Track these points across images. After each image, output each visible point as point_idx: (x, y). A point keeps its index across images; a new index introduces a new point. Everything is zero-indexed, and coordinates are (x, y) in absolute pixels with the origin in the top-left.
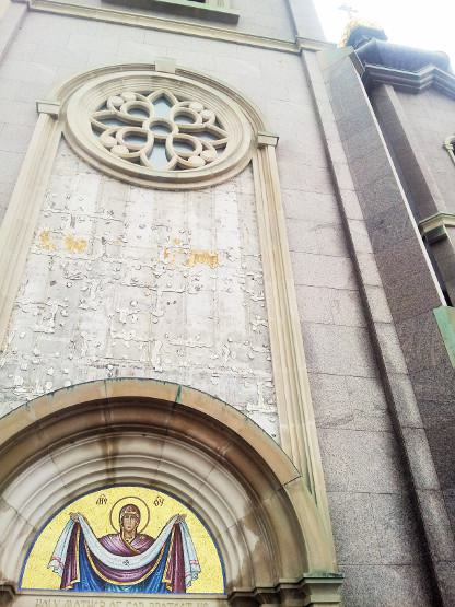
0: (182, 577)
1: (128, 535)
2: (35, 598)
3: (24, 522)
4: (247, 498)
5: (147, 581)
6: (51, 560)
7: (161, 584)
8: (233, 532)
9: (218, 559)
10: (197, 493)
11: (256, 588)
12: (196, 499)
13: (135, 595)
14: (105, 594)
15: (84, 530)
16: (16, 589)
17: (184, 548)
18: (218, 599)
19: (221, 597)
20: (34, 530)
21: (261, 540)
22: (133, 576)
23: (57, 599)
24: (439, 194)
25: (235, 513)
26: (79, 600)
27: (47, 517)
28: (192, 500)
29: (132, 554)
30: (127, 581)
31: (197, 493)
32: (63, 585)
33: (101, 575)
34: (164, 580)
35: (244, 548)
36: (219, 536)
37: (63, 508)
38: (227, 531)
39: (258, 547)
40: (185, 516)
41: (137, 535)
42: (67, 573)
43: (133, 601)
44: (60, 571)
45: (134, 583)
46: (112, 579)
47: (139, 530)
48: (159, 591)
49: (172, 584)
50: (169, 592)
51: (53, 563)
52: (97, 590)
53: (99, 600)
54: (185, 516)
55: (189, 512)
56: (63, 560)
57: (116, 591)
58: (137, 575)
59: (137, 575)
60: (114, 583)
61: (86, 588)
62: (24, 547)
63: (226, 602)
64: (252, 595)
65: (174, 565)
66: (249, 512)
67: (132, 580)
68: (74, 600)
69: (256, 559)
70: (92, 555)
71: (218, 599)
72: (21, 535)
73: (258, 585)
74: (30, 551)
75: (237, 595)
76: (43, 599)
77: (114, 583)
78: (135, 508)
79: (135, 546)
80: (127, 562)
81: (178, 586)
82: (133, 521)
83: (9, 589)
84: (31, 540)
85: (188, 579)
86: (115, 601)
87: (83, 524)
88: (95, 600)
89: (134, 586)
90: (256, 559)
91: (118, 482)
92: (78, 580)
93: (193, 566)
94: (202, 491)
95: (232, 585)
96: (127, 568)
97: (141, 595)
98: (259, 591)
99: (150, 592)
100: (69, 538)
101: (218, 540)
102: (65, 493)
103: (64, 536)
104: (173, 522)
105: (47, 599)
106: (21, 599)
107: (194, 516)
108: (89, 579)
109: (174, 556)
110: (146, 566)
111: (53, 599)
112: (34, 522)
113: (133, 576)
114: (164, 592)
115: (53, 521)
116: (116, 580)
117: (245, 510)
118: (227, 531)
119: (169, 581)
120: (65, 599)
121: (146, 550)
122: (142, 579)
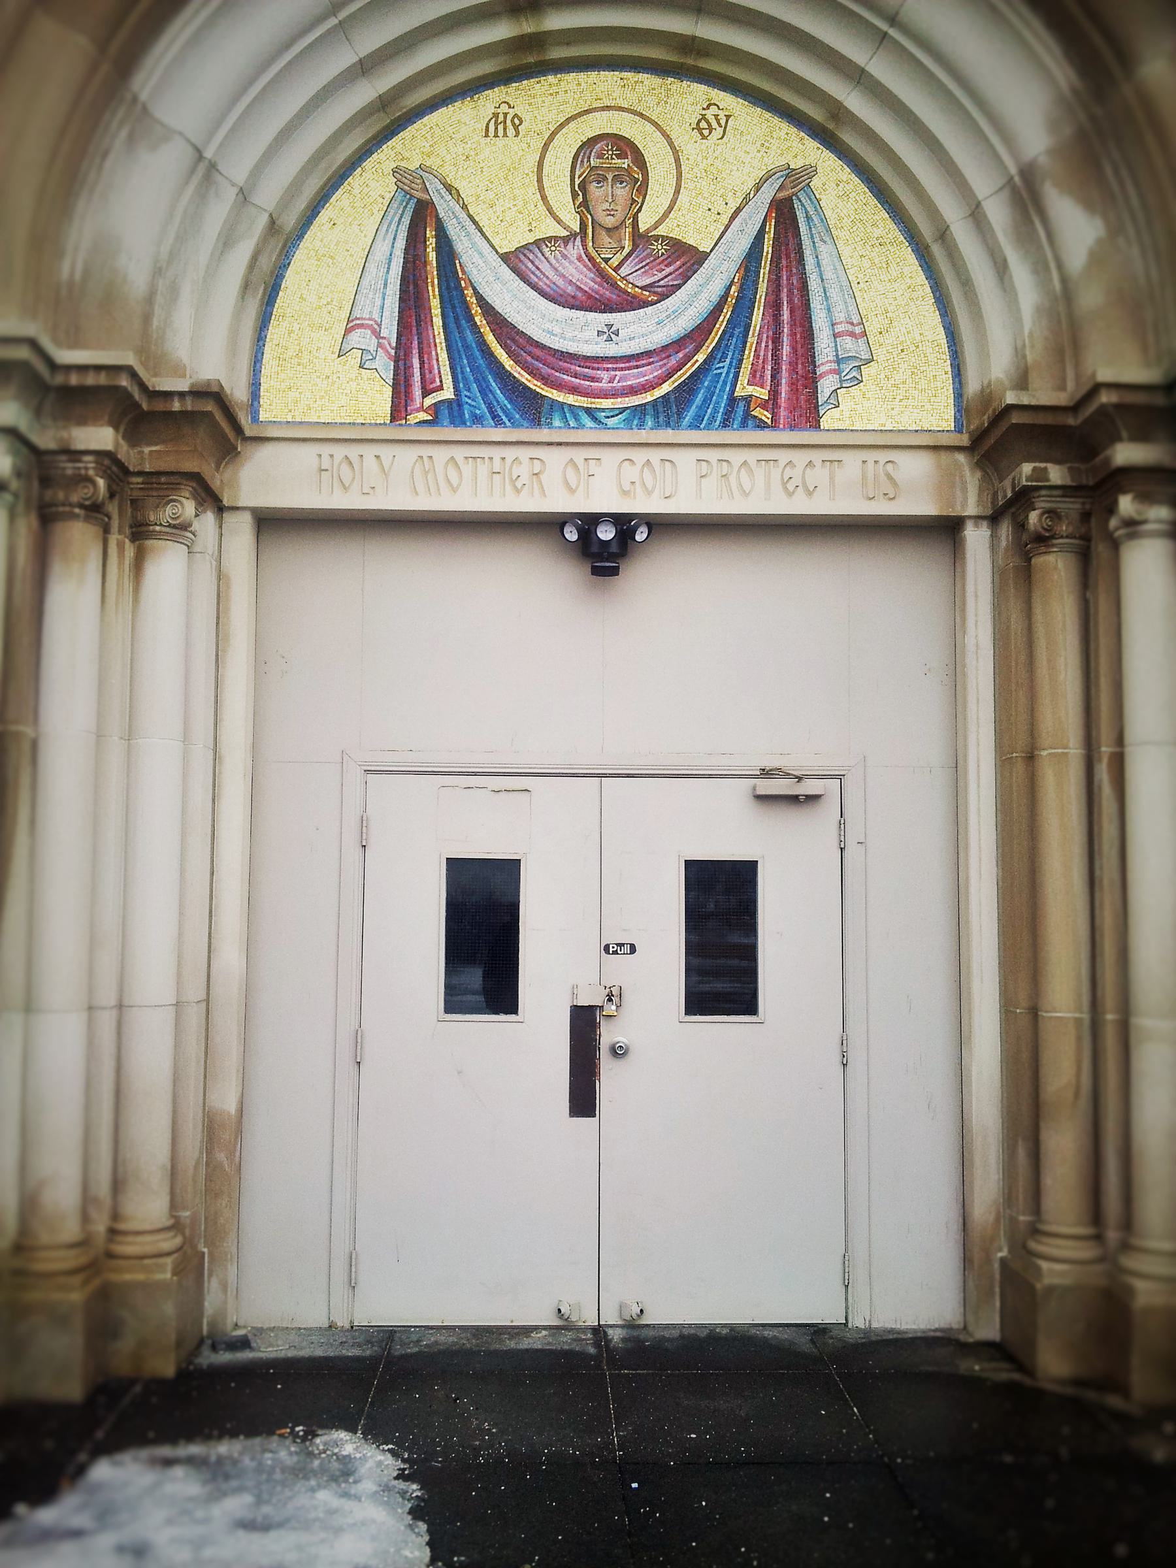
0: (808, 379)
1: (605, 239)
2: (311, 450)
3: (231, 194)
4: (1064, 74)
5: (686, 391)
6: (348, 331)
7: (732, 400)
8: (998, 213)
9: (933, 319)
10: (857, 76)
11: (1097, 388)
12: (855, 102)
13: (643, 435)
14: (543, 434)
15: (452, 230)
16: (244, 420)
17: (814, 284)
18: (935, 448)
19: (945, 440)
20: (273, 226)
21: (1115, 231)
22: (635, 377)
23: (386, 451)
24: (990, 411)
25: (1008, 139)
26: (459, 453)
27: (314, 184)
28: (838, 111)
29: (631, 303)
30: (614, 394)
31: (857, 76)
32: (399, 410)
33: (524, 377)
34: (744, 388)
35: (1040, 268)
36: (943, 235)
37: (365, 152)
38: (976, 215)
39: (1096, 258)
40: (810, 171)
41: (639, 239)
42: (408, 368)
43: (640, 456)
44: (385, 366)
45: (648, 397)
46: (559, 386)
47: (645, 221)
48: (726, 424)
49: (772, 403)
50: (761, 425)
51: (356, 338)
52: (515, 425)
53: (524, 453)
54: (810, 171)
55: (829, 165)
56: (390, 330)
57: (581, 426)
58: (650, 373)
59: (650, 373)
60: (571, 399)
61: (477, 420)
62: (246, 286)
63: (961, 458)
64: (1071, 421)
65: (776, 340)
66: (1068, 131)
67: (633, 391)
68: (441, 455)
69: (1091, 298)
70: (489, 310)
71: (935, 448)
72: (227, 241)
73: (1105, 374)
74: (270, 300)
75: (1016, 418)
76: (340, 451)
77: (571, 399)
78: (623, 145)
79: (634, 277)
80: (610, 333)
81: (792, 409)
82: (622, 192)
83: (210, 406)
84: (266, 263)
85: (826, 386)
86: (579, 455)
87: (444, 206)
88: (510, 453)
89: (640, 410)
90: (1091, 298)
91: (557, 53)
92: (448, 393)
93: (847, 343)
94: (880, 68)
95: (987, 396)
96: (612, 350)
97: (667, 435)
98: (1105, 398)
99: (695, 425)
100: (401, 243)
101: (937, 250)
102: (365, 93)
103: (382, 249)
104: (768, 194)
105: (353, 451)
106: (265, 453)
107: (846, 173)
108: (485, 391)
109: (774, 306)
110: (679, 344)
111: (369, 451)
112: (268, 196)
113: (635, 377)
114: (744, 425)
115: (340, 199)
116: (574, 390)
117: (1053, 126)
118: (976, 215)
119: (763, 393)
120: (412, 453)
121: (679, 287)
122: (666, 388)
